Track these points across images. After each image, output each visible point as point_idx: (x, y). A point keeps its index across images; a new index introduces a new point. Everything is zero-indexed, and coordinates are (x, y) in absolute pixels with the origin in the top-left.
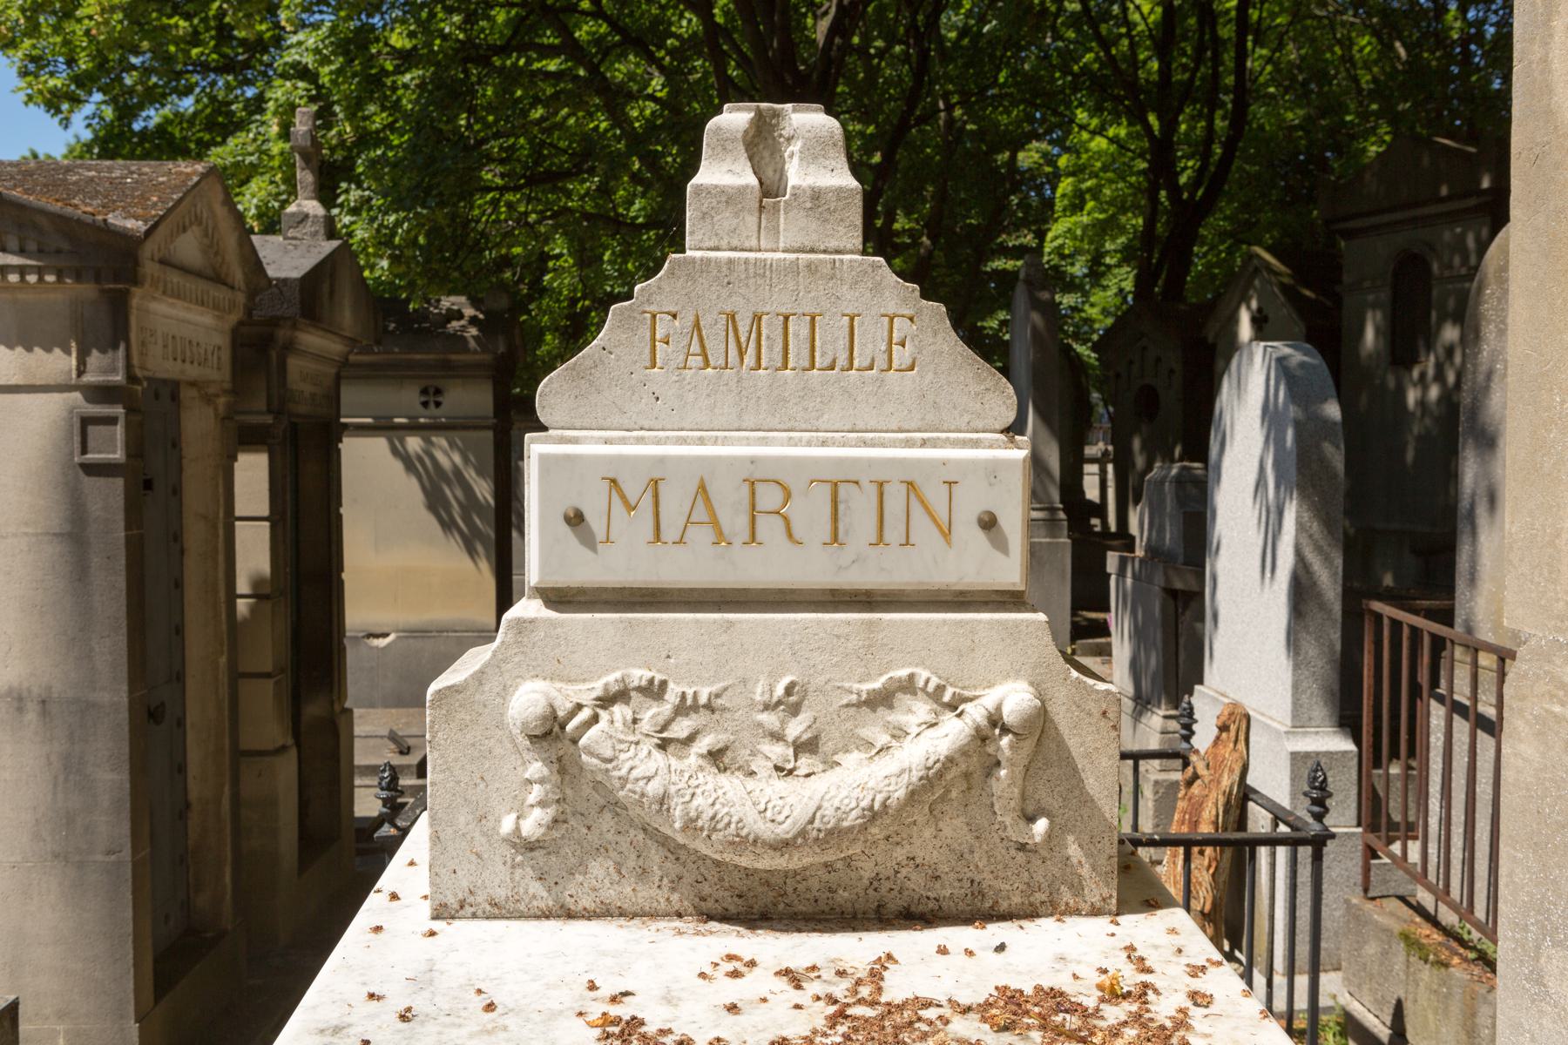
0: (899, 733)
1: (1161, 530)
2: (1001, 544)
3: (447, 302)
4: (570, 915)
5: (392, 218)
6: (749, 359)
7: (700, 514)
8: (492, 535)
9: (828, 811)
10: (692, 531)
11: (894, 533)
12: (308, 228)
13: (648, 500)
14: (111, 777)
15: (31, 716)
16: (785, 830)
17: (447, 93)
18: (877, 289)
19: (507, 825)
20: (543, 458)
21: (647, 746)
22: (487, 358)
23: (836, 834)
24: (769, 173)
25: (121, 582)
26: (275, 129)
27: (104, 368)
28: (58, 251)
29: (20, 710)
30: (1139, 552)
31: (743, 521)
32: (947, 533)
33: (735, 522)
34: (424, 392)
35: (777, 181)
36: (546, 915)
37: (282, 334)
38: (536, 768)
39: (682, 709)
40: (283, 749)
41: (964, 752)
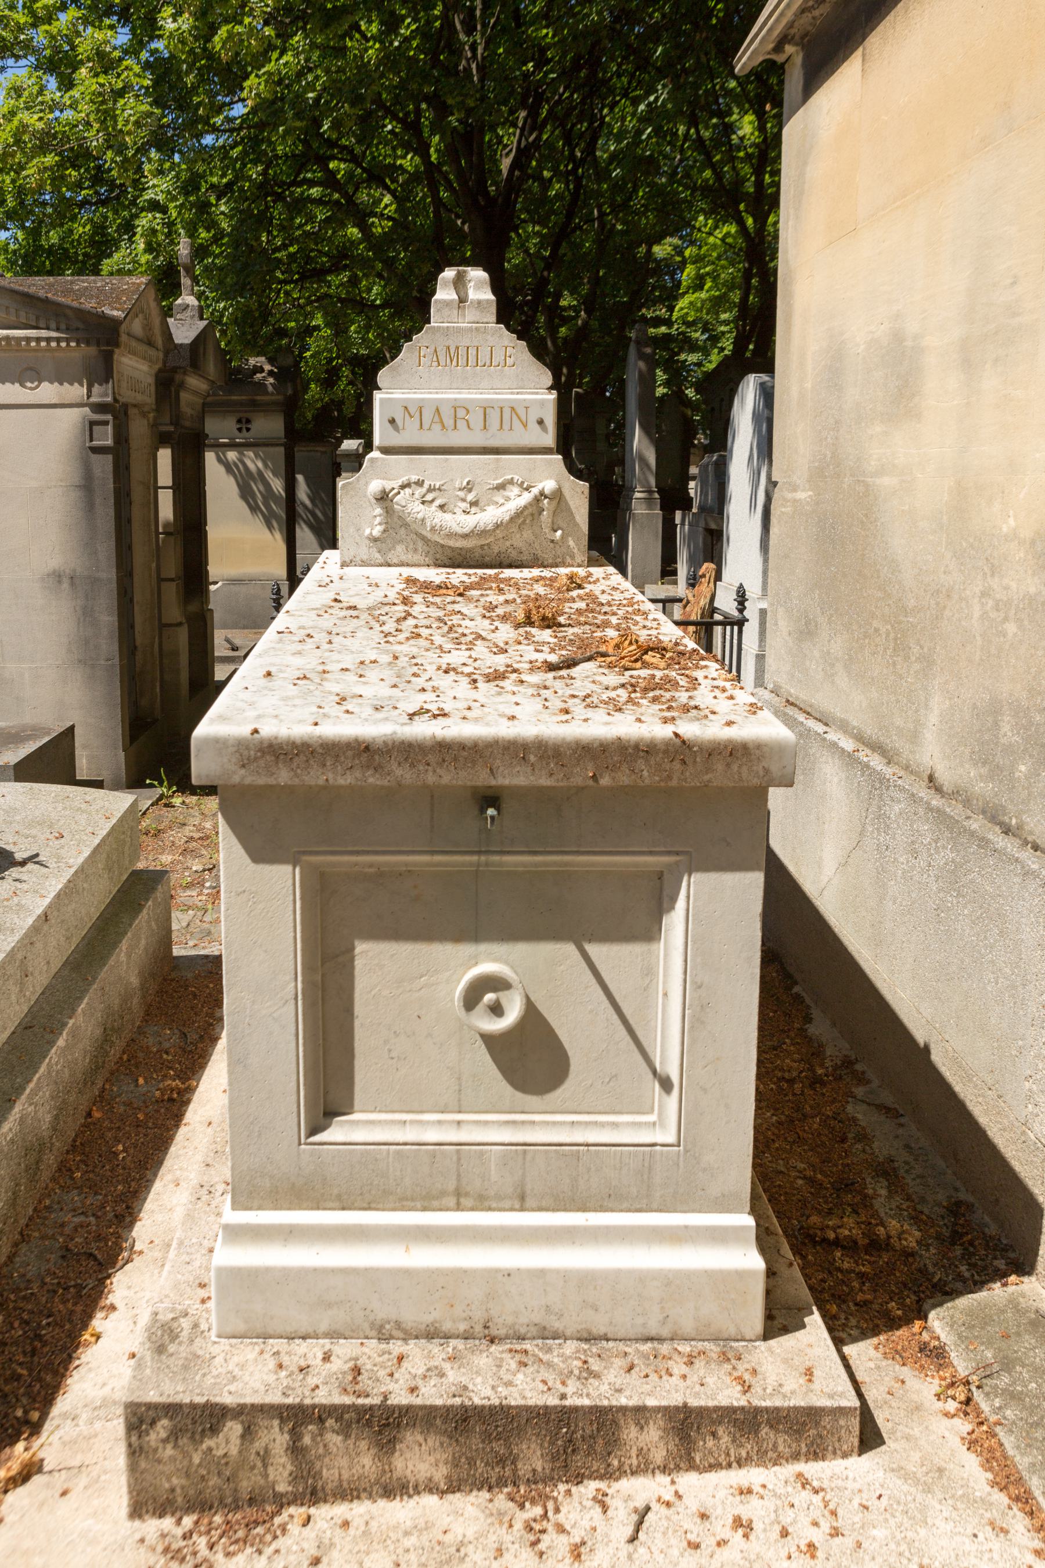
0: (508, 499)
1: (706, 495)
2: (545, 430)
3: (252, 361)
4: (389, 565)
5: (222, 305)
6: (454, 363)
7: (437, 419)
8: (284, 516)
9: (482, 524)
10: (434, 426)
11: (506, 426)
12: (189, 313)
13: (418, 414)
14: (108, 619)
15: (66, 585)
16: (466, 530)
17: (252, 221)
18: (501, 336)
19: (367, 532)
20: (381, 399)
21: (417, 502)
22: (280, 398)
23: (484, 533)
24: (462, 294)
25: (112, 512)
26: (142, 246)
27: (101, 394)
28: (77, 329)
29: (59, 582)
30: (695, 510)
31: (452, 422)
32: (525, 426)
33: (449, 422)
34: (239, 421)
35: (464, 294)
36: (381, 565)
37: (178, 377)
38: (378, 511)
39: (430, 490)
40: (180, 624)
41: (530, 504)
